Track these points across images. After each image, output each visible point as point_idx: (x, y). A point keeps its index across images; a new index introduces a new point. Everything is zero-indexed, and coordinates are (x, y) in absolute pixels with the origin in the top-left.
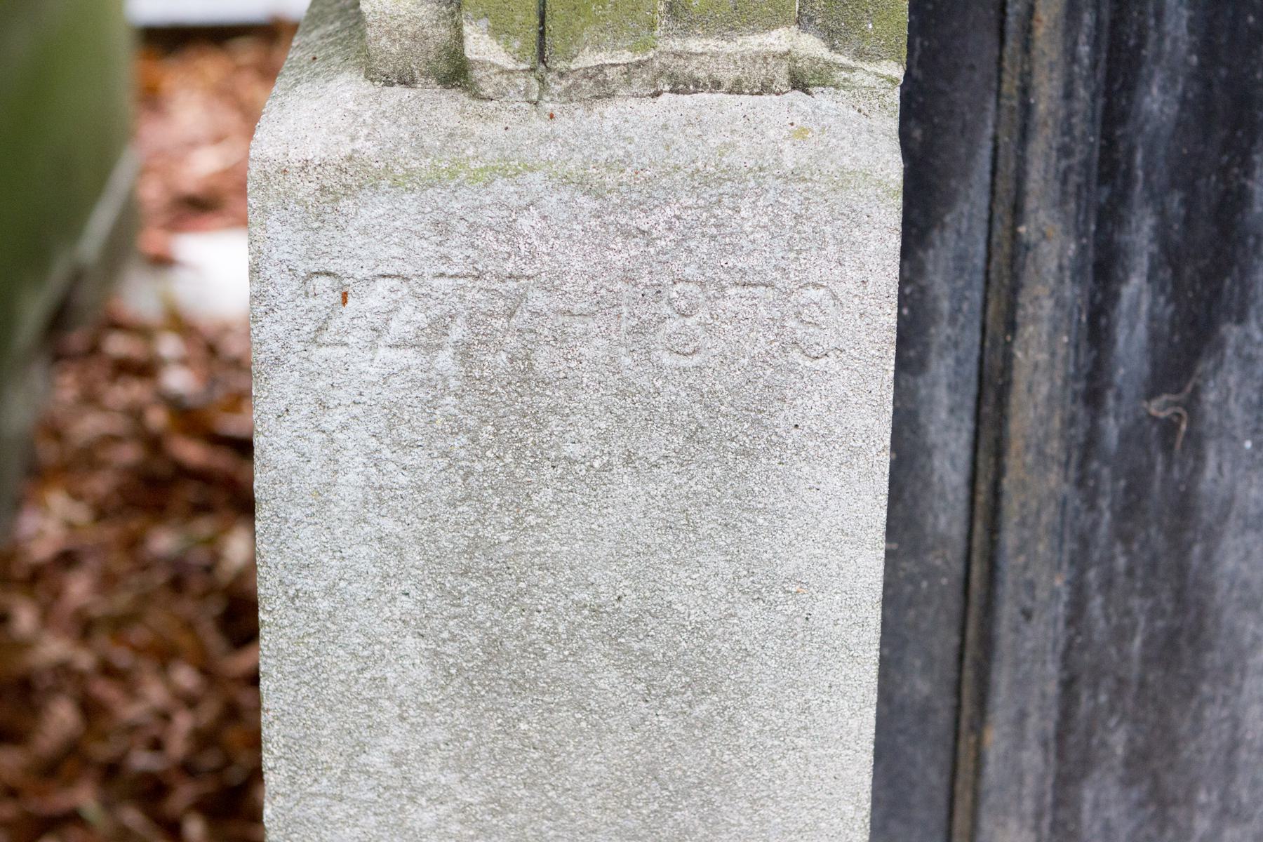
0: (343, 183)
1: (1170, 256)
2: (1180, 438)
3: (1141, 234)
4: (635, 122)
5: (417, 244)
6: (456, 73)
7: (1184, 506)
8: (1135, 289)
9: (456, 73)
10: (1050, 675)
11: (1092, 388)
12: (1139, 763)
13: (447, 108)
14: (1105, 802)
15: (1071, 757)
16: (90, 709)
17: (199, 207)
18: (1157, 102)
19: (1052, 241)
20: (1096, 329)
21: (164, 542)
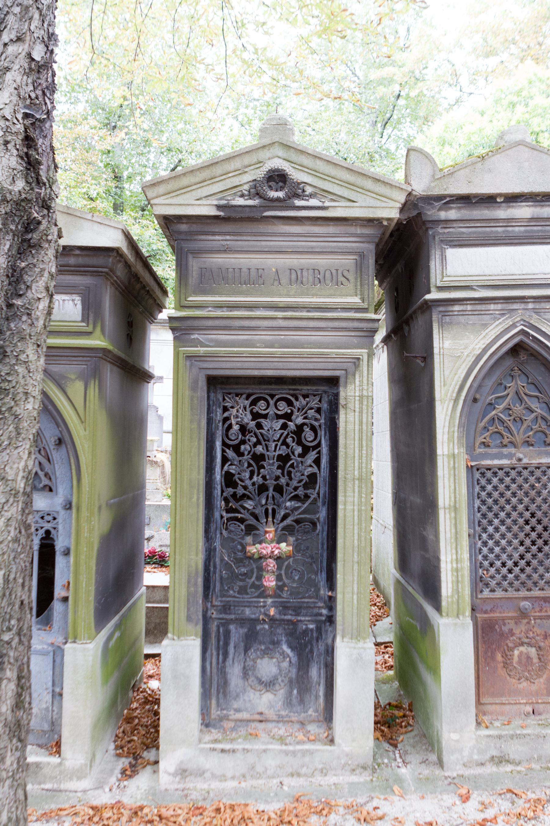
0: (167, 646)
1: (223, 654)
2: (224, 667)
3: (221, 652)
4: (184, 642)
5: (228, 816)
6: (174, 639)
7: (225, 672)
8: (221, 656)
9: (174, 639)
10: (216, 686)
11: (218, 663)
12: (223, 693)
13: (173, 642)
14: (221, 695)
15: (218, 692)
16: (139, 721)
17: (151, 677)
18: (221, 643)
19: (215, 653)
20: (218, 659)
21: (147, 707)
